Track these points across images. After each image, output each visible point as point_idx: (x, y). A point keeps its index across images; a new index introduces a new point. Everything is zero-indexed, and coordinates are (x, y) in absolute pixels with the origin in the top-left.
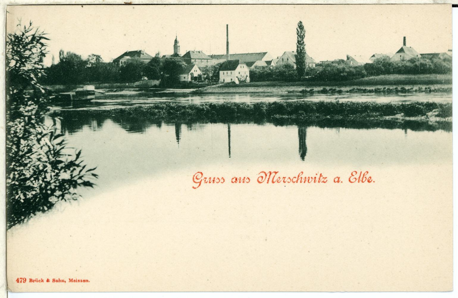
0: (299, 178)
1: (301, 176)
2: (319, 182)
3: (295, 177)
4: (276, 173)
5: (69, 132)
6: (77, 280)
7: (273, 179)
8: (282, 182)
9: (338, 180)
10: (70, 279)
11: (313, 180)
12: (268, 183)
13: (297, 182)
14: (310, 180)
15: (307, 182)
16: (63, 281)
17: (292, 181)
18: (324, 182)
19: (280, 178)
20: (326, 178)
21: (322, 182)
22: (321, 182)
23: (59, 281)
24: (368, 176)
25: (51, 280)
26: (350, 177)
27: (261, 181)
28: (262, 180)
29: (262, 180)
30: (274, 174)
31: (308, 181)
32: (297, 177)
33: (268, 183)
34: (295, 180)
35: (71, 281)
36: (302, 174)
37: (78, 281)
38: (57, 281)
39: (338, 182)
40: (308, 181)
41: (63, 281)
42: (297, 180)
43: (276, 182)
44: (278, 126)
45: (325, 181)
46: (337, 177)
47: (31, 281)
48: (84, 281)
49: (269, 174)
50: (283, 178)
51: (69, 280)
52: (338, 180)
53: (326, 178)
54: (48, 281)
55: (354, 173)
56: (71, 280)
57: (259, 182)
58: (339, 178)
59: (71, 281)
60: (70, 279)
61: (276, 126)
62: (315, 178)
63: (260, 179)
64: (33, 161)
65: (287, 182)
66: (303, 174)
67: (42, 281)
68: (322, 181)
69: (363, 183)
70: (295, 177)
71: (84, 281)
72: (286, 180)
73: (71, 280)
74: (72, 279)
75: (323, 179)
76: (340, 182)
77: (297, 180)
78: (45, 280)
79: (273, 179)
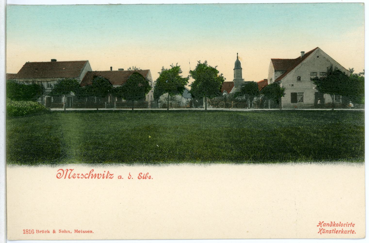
0: (91, 174)
1: (92, 173)
2: (107, 178)
3: (87, 174)
4: (71, 170)
5: (115, 165)
6: (82, 231)
7: (69, 175)
8: (77, 178)
9: (120, 177)
10: (75, 230)
11: (102, 177)
12: (65, 178)
13: (88, 178)
14: (100, 176)
15: (97, 177)
16: (69, 232)
17: (85, 177)
18: (111, 178)
19: (75, 174)
20: (113, 174)
21: (109, 178)
22: (108, 178)
23: (65, 231)
24: (148, 176)
25: (57, 231)
26: (139, 177)
27: (59, 177)
28: (60, 176)
29: (60, 176)
30: (70, 171)
31: (98, 177)
32: (89, 173)
33: (65, 178)
34: (87, 176)
35: (76, 232)
36: (93, 171)
38: (63, 232)
39: (121, 178)
40: (98, 177)
41: (69, 232)
42: (89, 177)
43: (72, 178)
44: (50, 61)
45: (112, 177)
46: (120, 176)
47: (38, 232)
48: (88, 232)
49: (66, 170)
50: (78, 174)
52: (120, 177)
53: (113, 174)
54: (54, 232)
55: (140, 174)
56: (76, 231)
57: (58, 177)
58: (121, 176)
59: (76, 232)
60: (75, 230)
61: (54, 61)
62: (104, 174)
63: (59, 175)
64: (351, 230)
65: (80, 177)
66: (94, 171)
67: (49, 232)
68: (109, 177)
69: (130, 179)
70: (87, 174)
71: (88, 232)
72: (80, 176)
73: (76, 231)
74: (77, 230)
75: (110, 176)
76: (122, 178)
77: (89, 177)
78: (51, 231)
79: (69, 175)
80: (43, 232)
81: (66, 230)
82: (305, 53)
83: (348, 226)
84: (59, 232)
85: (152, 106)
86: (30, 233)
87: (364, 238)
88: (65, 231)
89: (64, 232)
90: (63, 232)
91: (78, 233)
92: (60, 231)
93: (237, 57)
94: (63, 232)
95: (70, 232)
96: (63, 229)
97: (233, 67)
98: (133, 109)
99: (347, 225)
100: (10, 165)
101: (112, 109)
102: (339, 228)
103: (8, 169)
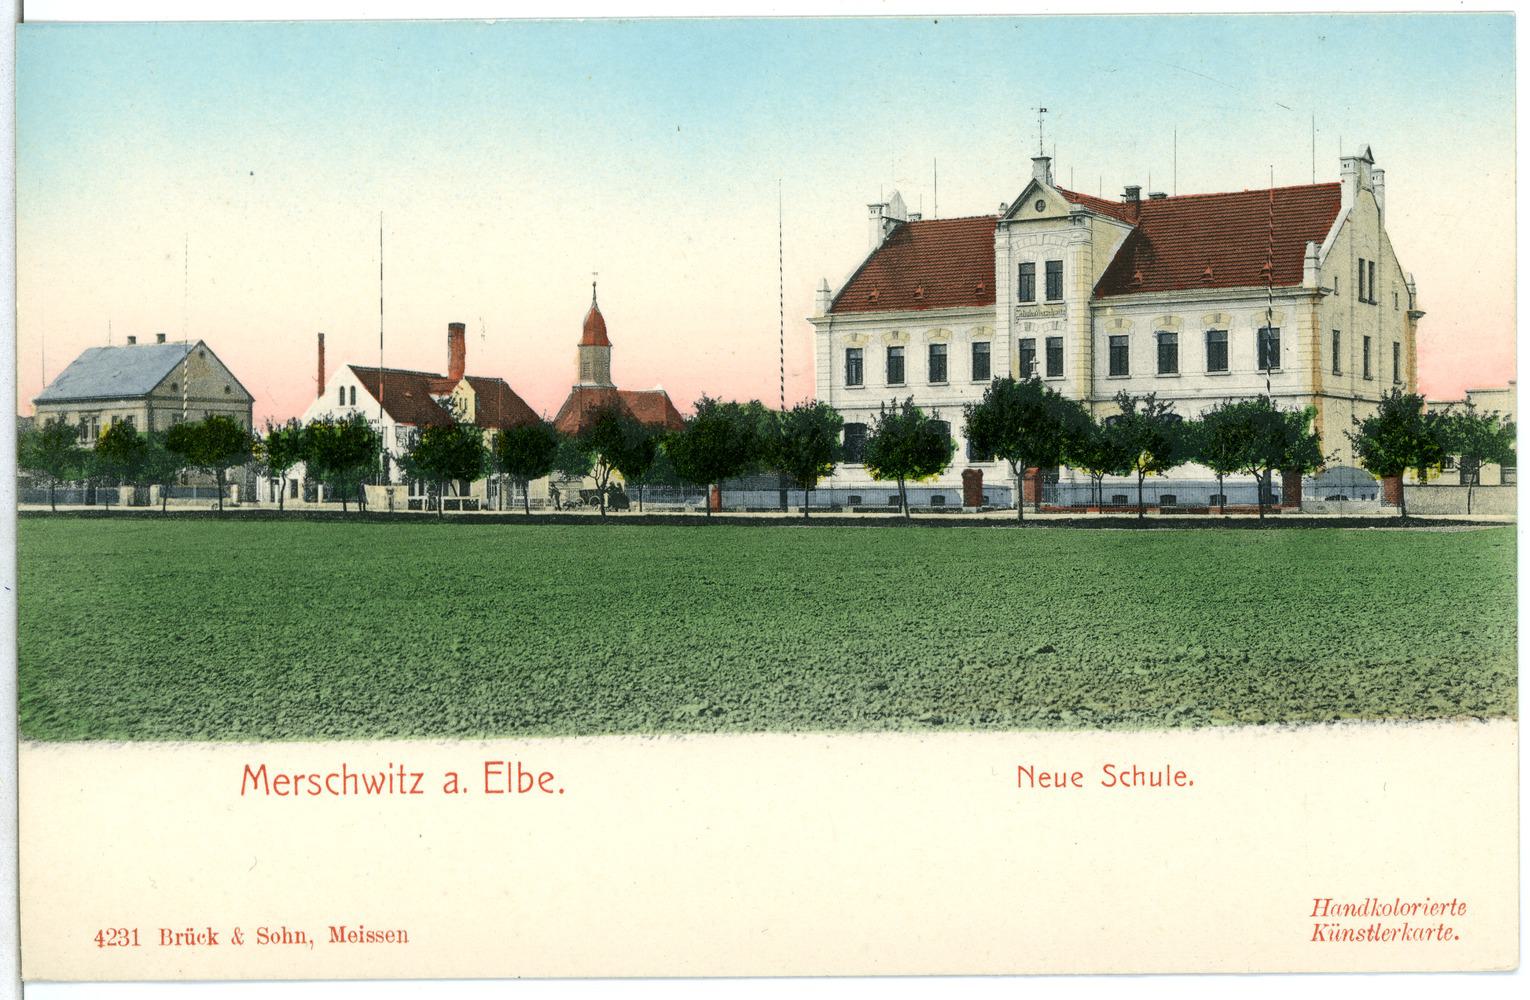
16: (300, 938)
23: (285, 937)
25: (249, 938)
37: (365, 937)
41: (300, 938)
51: (328, 934)
54: (237, 939)
56: (338, 935)
73: (338, 935)
78: (320, 933)
80: (190, 941)
81: (287, 931)
82: (922, 219)
83: (178, 943)
84: (233, 941)
85: (485, 507)
86: (400, 941)
87: (1512, 972)
88: (285, 937)
89: (279, 938)
90: (275, 938)
91: (348, 942)
92: (263, 936)
93: (595, 298)
94: (275, 938)
95: (307, 940)
96: (275, 928)
97: (578, 335)
98: (1141, 516)
99: (187, 935)
100: (29, 744)
101: (1277, 516)
102: (1391, 922)
103: (25, 747)
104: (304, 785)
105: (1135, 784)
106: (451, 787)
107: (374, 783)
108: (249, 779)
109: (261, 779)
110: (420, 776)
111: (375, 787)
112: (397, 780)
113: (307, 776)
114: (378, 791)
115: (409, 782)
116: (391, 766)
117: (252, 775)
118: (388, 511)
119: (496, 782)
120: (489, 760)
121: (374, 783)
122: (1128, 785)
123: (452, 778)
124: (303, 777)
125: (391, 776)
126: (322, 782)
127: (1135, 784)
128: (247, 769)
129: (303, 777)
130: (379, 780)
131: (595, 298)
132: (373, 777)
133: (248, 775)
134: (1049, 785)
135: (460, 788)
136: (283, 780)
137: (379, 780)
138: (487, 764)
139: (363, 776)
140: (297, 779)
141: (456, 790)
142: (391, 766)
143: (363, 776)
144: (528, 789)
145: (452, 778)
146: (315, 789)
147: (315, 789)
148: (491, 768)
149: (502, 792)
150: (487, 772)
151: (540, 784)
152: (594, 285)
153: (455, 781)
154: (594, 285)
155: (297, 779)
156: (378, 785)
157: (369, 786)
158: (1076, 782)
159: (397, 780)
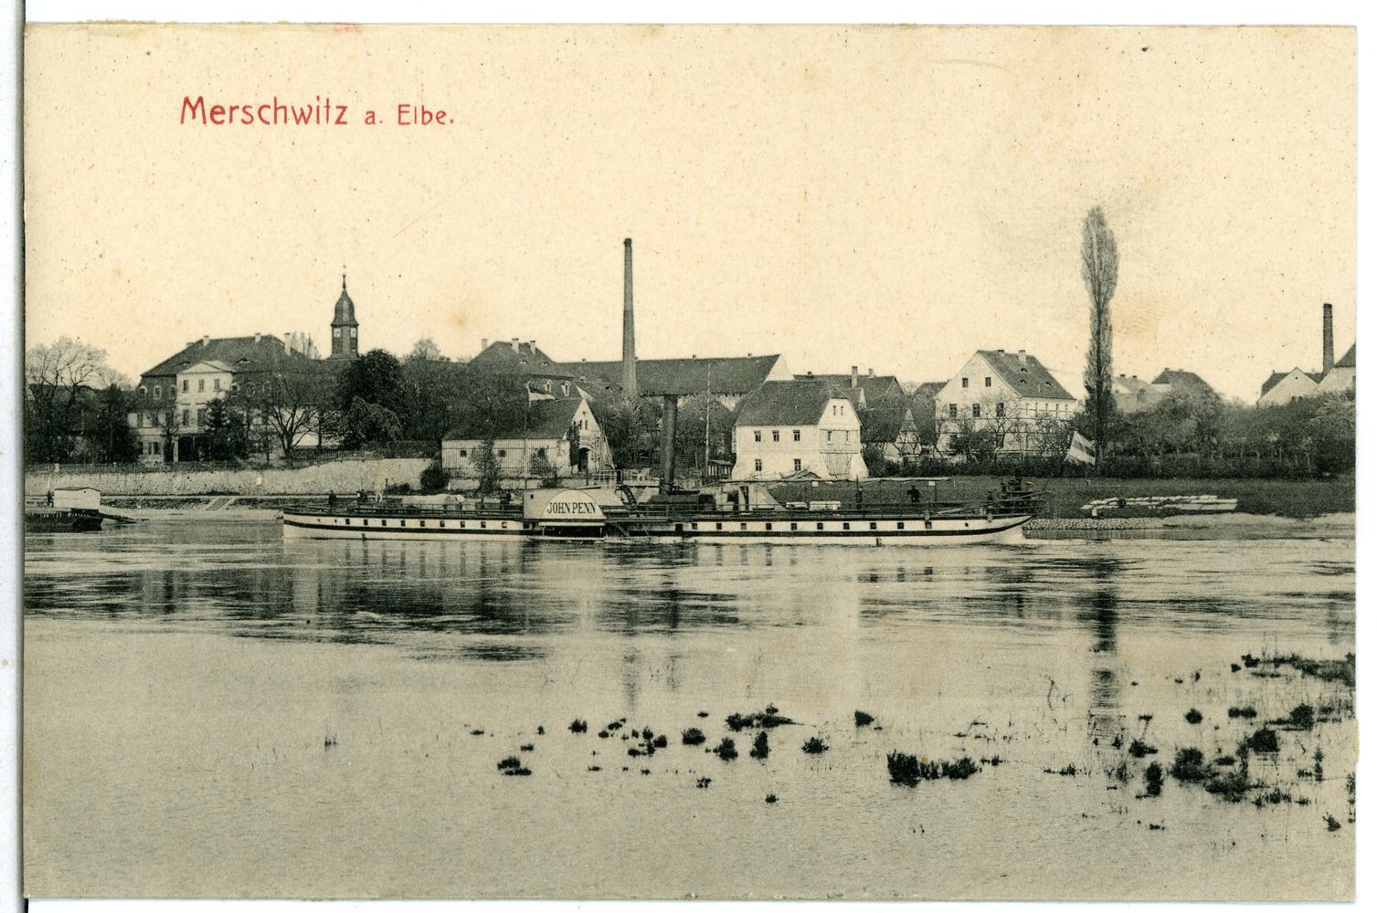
54: (371, 117)
104: (238, 114)
105: (276, 122)
106: (370, 120)
107: (303, 114)
108: (188, 109)
109: (199, 112)
110: (344, 108)
111: (302, 118)
112: (323, 111)
113: (241, 107)
114: (306, 122)
115: (334, 113)
116: (318, 98)
117: (191, 106)
118: (499, 444)
119: (405, 118)
120: (401, 103)
121: (303, 114)
122: (268, 123)
123: (370, 115)
124: (237, 107)
125: (318, 107)
126: (254, 112)
127: (276, 122)
128: (187, 101)
129: (237, 107)
130: (307, 111)
131: (344, 287)
132: (302, 109)
133: (187, 106)
134: (222, 122)
135: (377, 120)
136: (218, 110)
137: (307, 111)
138: (400, 106)
139: (293, 108)
140: (232, 109)
141: (373, 122)
142: (318, 98)
143: (293, 108)
144: (429, 121)
145: (370, 115)
146: (247, 118)
147: (247, 118)
148: (403, 109)
149: (409, 123)
150: (400, 112)
151: (438, 118)
152: (344, 277)
153: (373, 116)
154: (344, 277)
155: (232, 109)
156: (306, 116)
157: (298, 117)
158: (440, 120)
159: (323, 111)
